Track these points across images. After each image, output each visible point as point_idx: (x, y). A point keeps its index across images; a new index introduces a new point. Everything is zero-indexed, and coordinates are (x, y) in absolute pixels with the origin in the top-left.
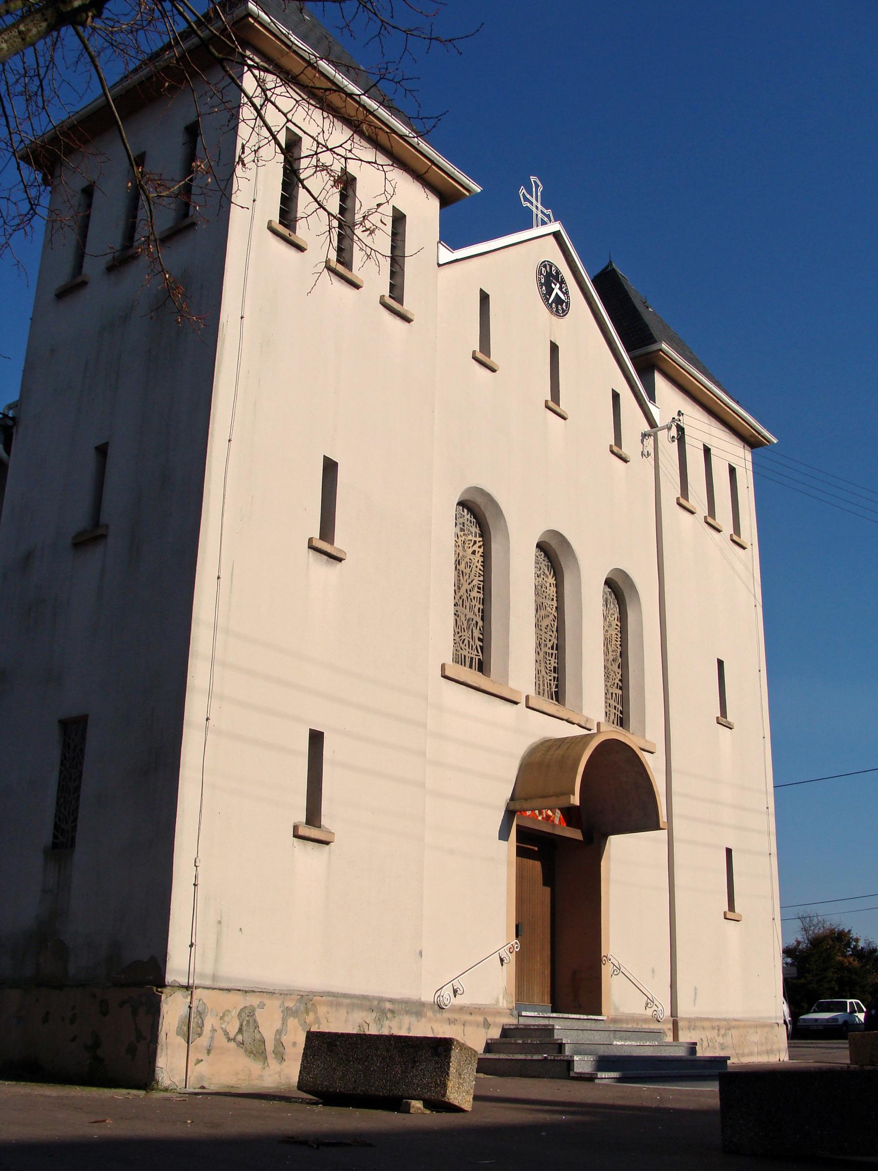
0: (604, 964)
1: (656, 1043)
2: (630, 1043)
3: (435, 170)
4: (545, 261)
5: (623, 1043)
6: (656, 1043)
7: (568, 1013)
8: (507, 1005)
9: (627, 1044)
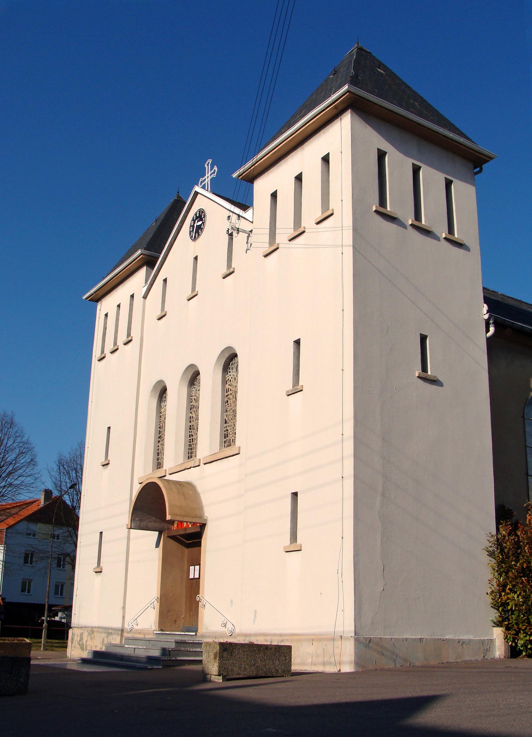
0: (200, 602)
1: (145, 647)
2: (132, 647)
3: (329, 109)
4: (201, 209)
5: (129, 646)
6: (145, 647)
7: (175, 632)
8: (155, 628)
9: (130, 647)
